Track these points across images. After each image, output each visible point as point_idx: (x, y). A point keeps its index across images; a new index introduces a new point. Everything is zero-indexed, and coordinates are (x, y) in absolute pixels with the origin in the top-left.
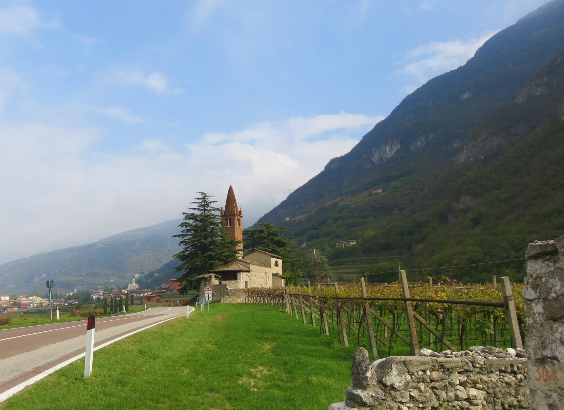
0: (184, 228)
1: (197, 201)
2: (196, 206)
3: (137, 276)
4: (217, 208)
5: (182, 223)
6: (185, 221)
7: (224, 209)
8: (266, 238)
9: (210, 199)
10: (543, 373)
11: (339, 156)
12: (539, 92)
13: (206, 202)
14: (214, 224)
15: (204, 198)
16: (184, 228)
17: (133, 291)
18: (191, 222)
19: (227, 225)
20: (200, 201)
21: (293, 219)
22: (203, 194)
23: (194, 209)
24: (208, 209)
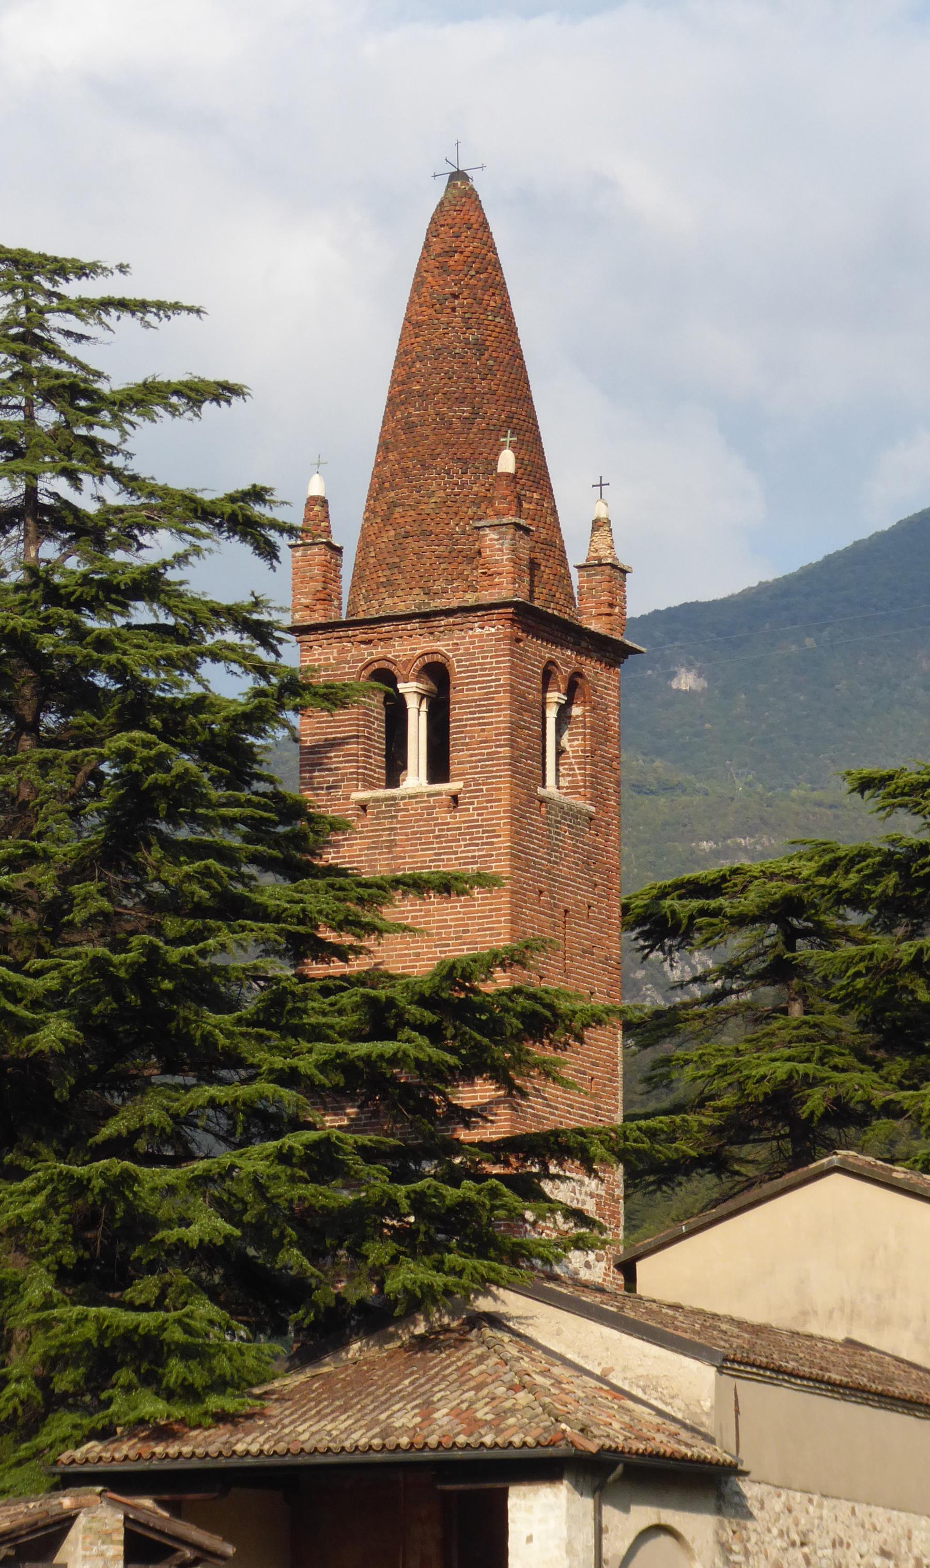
4: (214, 487)
9: (117, 355)
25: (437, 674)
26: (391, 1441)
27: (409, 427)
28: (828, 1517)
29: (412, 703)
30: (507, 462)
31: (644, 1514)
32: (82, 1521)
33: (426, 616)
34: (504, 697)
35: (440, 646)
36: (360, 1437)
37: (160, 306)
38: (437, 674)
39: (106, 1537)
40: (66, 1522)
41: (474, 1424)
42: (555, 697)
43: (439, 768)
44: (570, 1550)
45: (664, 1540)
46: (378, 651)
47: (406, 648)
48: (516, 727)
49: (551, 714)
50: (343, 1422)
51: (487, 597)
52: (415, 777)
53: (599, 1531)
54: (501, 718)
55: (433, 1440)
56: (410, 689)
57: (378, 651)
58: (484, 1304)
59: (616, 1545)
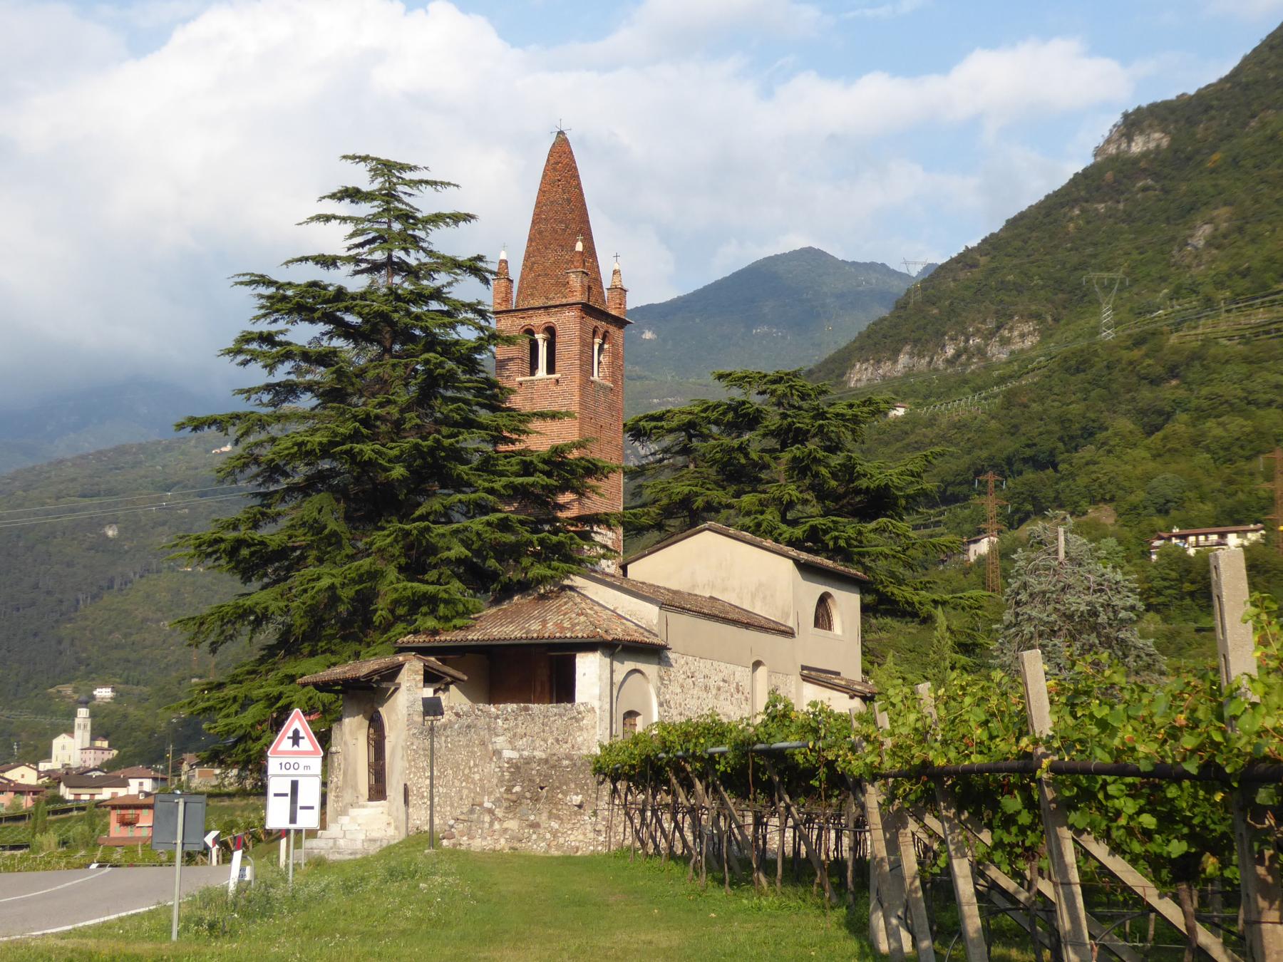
0: (257, 375)
1: (345, 208)
2: (335, 239)
3: (103, 693)
5: (247, 338)
6: (264, 327)
7: (515, 272)
8: (780, 444)
9: (424, 202)
10: (678, 827)
11: (1171, 95)
12: (800, 759)
13: (407, 217)
14: (448, 349)
15: (389, 196)
16: (257, 375)
17: (77, 777)
18: (303, 333)
19: (533, 373)
20: (365, 209)
21: (923, 412)
22: (385, 168)
23: (328, 262)
24: (413, 259)
25: (551, 331)
26: (530, 635)
27: (540, 233)
28: (703, 666)
29: (540, 342)
30: (579, 247)
31: (630, 665)
32: (407, 666)
33: (546, 308)
34: (577, 340)
35: (552, 320)
36: (518, 634)
37: (442, 183)
38: (551, 331)
39: (416, 672)
40: (400, 666)
41: (563, 629)
42: (598, 340)
43: (551, 368)
44: (600, 679)
45: (638, 675)
46: (527, 322)
47: (539, 320)
48: (582, 352)
49: (596, 347)
50: (511, 628)
51: (571, 300)
52: (542, 372)
53: (612, 672)
54: (576, 349)
55: (546, 635)
56: (540, 337)
57: (527, 322)
58: (566, 582)
59: (618, 677)
